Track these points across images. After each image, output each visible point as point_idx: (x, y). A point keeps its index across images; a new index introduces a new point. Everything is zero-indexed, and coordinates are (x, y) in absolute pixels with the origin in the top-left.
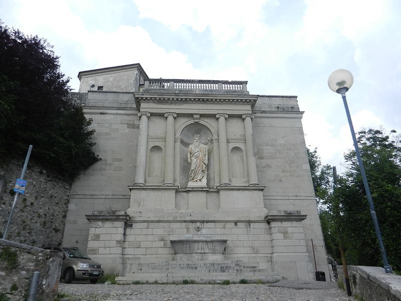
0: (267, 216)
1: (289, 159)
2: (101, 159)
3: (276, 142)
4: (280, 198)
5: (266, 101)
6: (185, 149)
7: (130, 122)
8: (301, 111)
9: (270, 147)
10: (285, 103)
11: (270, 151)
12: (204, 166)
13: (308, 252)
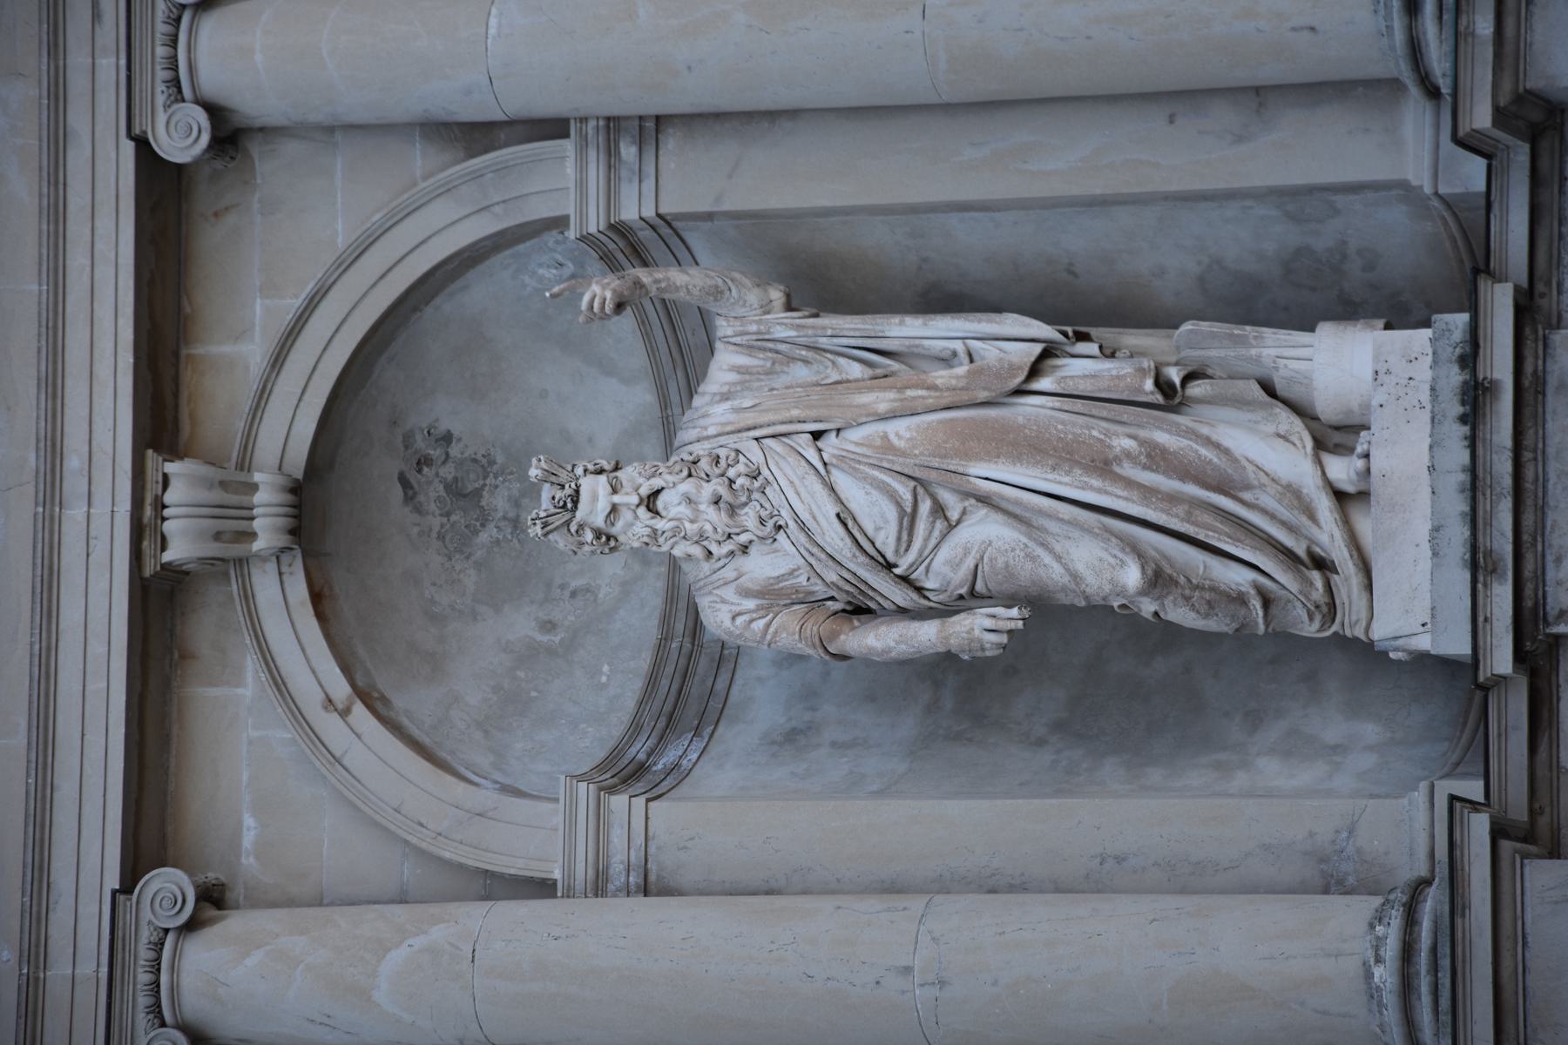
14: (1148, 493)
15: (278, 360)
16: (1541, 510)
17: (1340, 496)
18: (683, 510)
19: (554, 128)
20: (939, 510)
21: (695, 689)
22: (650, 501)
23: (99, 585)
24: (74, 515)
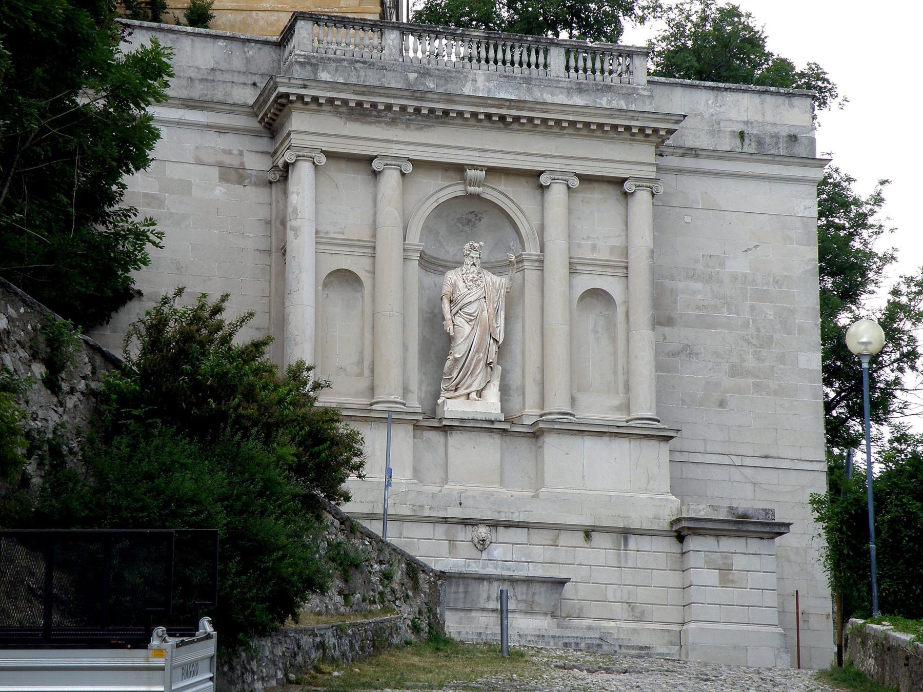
0: (679, 520)
1: (758, 330)
2: (140, 293)
3: (722, 264)
4: (715, 459)
5: (701, 108)
6: (430, 279)
7: (228, 160)
8: (818, 156)
9: (699, 286)
10: (769, 118)
11: (700, 297)
12: (494, 348)
13: (781, 624)
14: (472, 359)
15: (501, 193)
16: (470, 431)
17: (468, 394)
18: (472, 271)
19: (542, 250)
20: (471, 320)
21: (431, 266)
22: (474, 264)
23: (464, 158)
24: (477, 154)
